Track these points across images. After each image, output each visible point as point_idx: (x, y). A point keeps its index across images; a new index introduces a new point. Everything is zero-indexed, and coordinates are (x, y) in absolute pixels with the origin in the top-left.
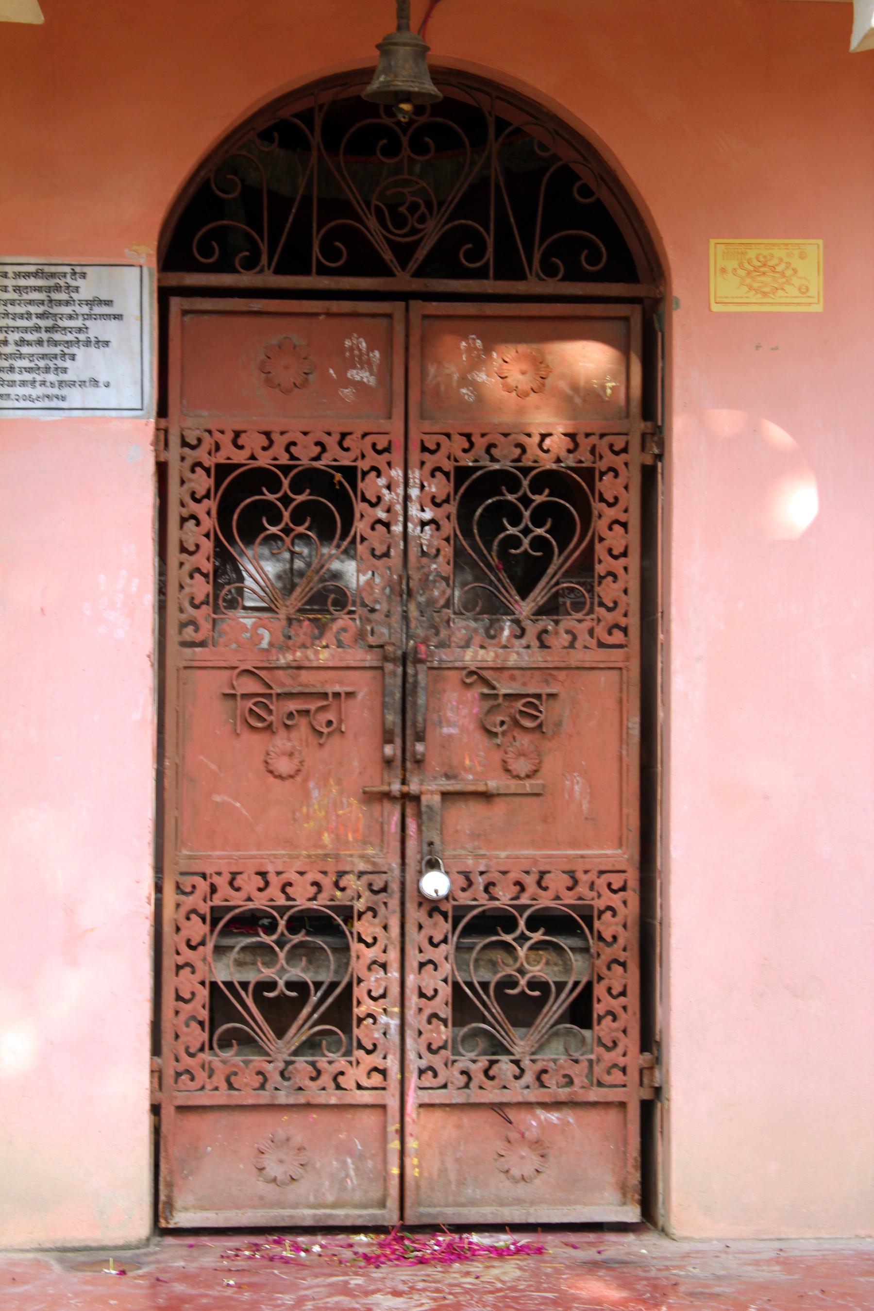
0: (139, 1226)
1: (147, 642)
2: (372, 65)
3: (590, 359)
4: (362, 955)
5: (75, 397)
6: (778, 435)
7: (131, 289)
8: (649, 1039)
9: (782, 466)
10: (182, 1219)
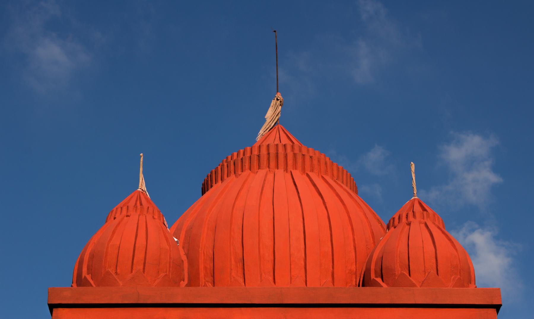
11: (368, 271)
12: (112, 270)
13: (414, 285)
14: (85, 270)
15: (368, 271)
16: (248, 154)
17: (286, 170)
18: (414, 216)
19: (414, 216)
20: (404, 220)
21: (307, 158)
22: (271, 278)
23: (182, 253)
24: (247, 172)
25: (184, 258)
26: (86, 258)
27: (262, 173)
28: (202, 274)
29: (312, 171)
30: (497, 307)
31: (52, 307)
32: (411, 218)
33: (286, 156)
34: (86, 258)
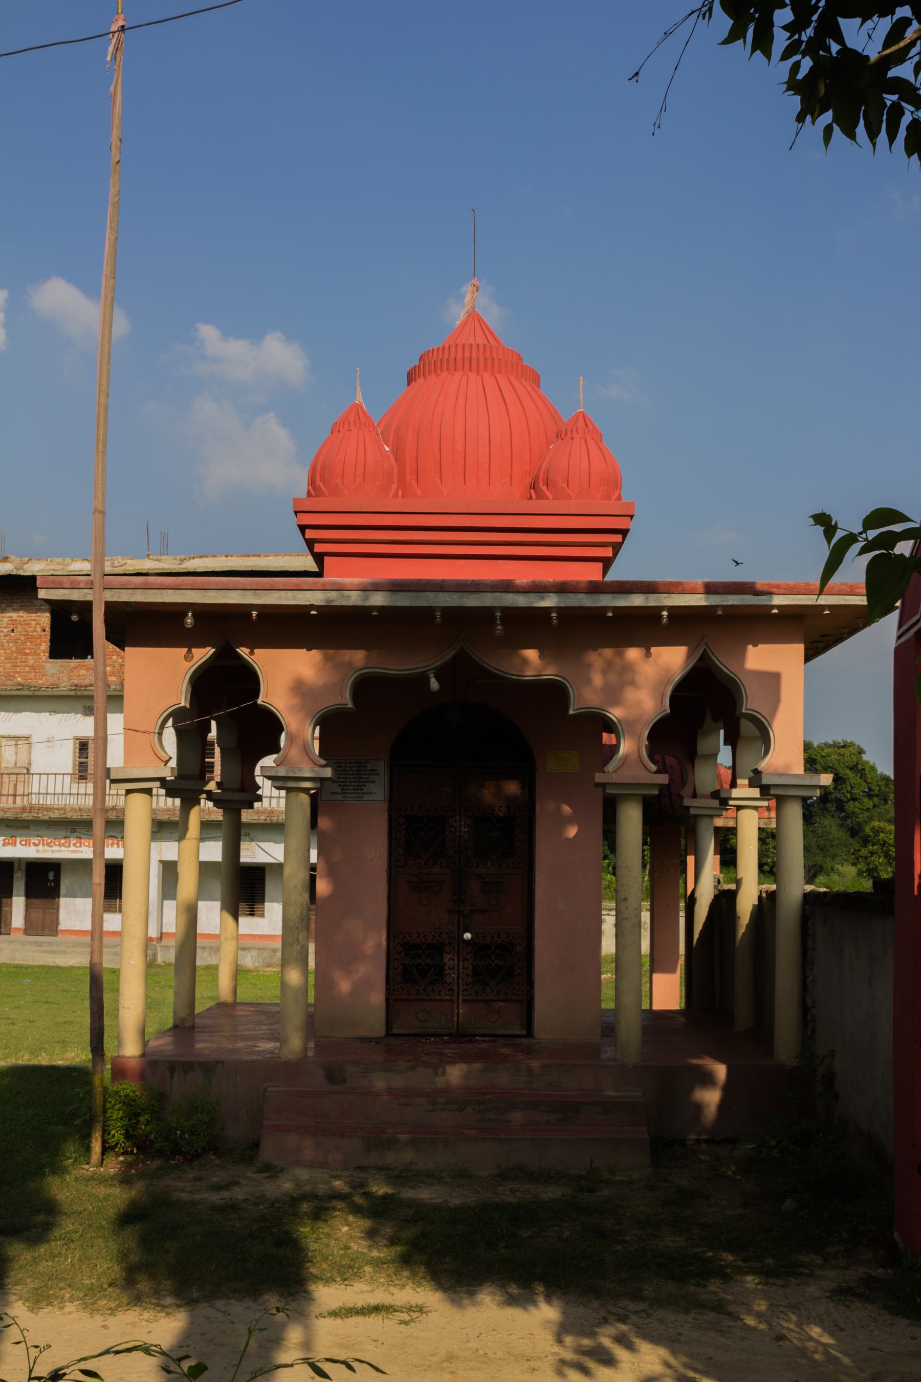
0: (382, 1033)
1: (385, 867)
2: (163, 839)
3: (512, 788)
4: (447, 958)
5: (366, 797)
6: (566, 809)
7: (382, 767)
8: (530, 983)
9: (568, 821)
10: (395, 1031)
11: (536, 479)
12: (338, 481)
13: (570, 498)
14: (318, 477)
15: (536, 479)
16: (446, 356)
17: (478, 373)
18: (577, 431)
19: (577, 431)
20: (569, 435)
21: (496, 361)
22: (462, 479)
23: (392, 459)
24: (445, 374)
25: (394, 464)
26: (319, 467)
27: (458, 375)
28: (408, 472)
29: (500, 372)
30: (632, 517)
31: (296, 513)
32: (575, 434)
33: (478, 359)
34: (319, 467)
